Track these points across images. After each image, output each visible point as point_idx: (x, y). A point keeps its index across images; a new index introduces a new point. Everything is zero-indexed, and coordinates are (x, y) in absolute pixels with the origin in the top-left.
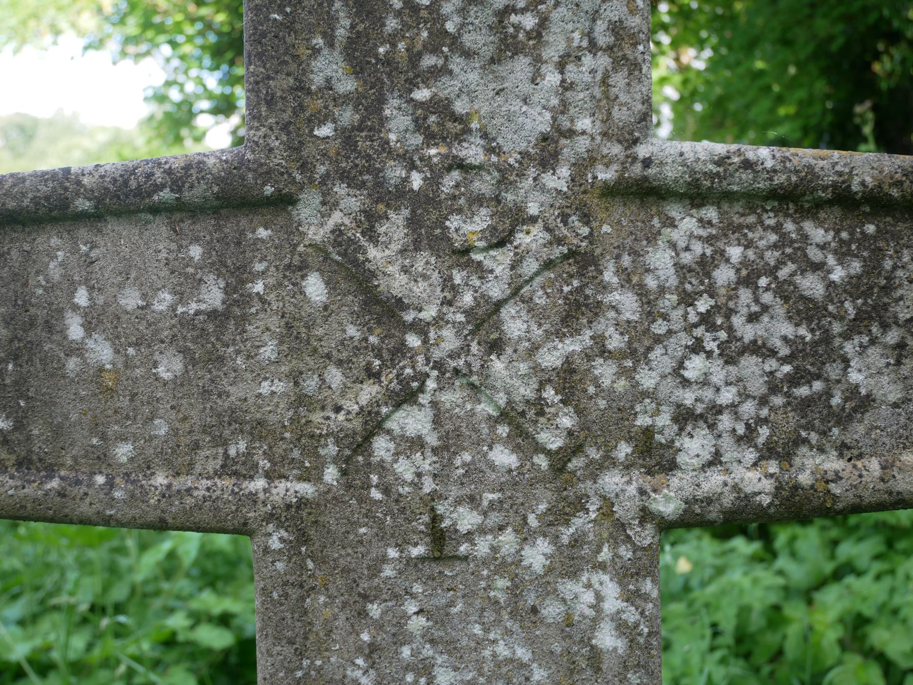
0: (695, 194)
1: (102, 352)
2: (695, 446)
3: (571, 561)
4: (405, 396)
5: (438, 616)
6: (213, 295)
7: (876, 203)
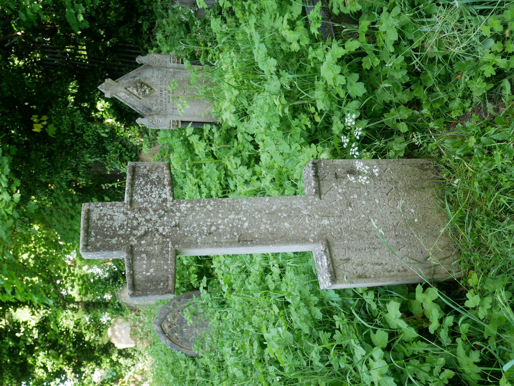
0: (131, 196)
1: (152, 270)
2: (164, 196)
3: (179, 210)
4: (157, 230)
6: (144, 255)
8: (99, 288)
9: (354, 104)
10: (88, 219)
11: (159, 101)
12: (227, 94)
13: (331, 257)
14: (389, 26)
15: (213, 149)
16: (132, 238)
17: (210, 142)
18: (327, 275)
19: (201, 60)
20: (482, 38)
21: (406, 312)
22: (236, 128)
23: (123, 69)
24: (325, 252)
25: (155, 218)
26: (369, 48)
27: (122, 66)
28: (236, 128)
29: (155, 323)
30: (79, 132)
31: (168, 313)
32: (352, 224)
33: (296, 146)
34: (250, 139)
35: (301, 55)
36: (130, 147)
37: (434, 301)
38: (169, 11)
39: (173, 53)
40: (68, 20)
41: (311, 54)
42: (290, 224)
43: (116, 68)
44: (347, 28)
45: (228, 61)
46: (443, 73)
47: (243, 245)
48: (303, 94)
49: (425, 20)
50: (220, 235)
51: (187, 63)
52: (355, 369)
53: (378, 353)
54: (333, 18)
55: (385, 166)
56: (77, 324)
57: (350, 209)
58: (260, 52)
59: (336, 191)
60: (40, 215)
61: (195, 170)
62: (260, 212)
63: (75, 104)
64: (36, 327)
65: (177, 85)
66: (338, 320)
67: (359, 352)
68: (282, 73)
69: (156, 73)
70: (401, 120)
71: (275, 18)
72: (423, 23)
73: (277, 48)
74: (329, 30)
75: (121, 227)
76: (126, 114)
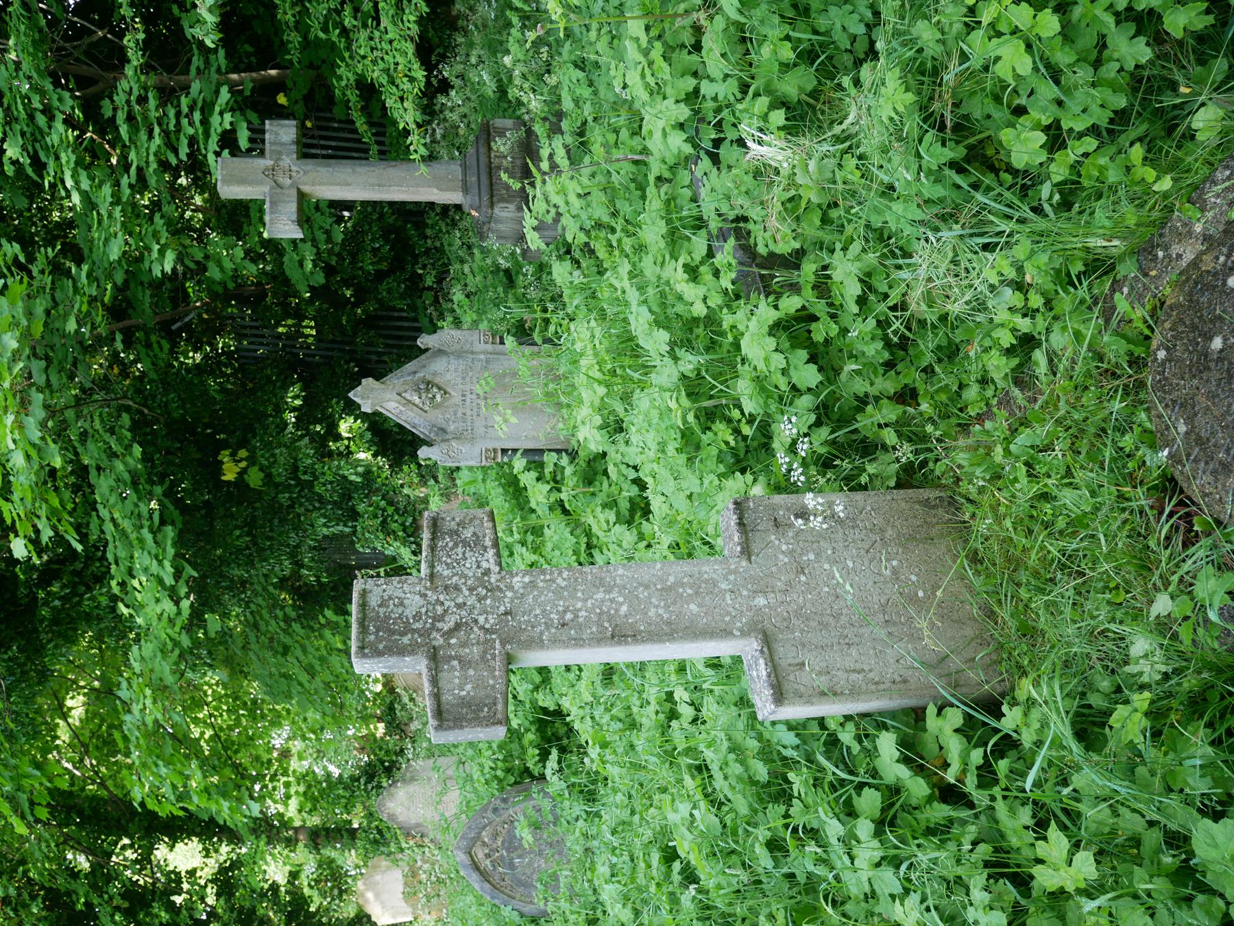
0: (432, 566)
1: (468, 687)
2: (484, 565)
3: (511, 588)
4: (476, 621)
5: (524, 614)
6: (455, 663)
7: (434, 533)
8: (339, 797)
9: (806, 401)
10: (363, 605)
11: (459, 414)
12: (586, 395)
13: (772, 660)
14: (846, 274)
15: (564, 496)
16: (434, 634)
17: (556, 483)
18: (768, 692)
19: (537, 337)
20: (992, 288)
21: (911, 754)
22: (604, 454)
23: (386, 358)
24: (762, 651)
25: (471, 601)
26: (820, 308)
27: (384, 354)
28: (604, 454)
29: (458, 848)
30: (306, 477)
31: (484, 828)
32: (814, 610)
33: (710, 479)
34: (632, 474)
35: (711, 320)
36: (401, 506)
37: (956, 731)
38: (476, 251)
39: (484, 326)
40: (288, 273)
41: (727, 320)
42: (700, 606)
43: (374, 357)
44: (780, 276)
45: (584, 336)
46: (944, 343)
47: (619, 643)
48: (714, 387)
49: (901, 261)
50: (580, 627)
51: (510, 341)
52: (837, 878)
53: (864, 828)
54: (758, 260)
55: (861, 503)
56: (294, 875)
57: (803, 578)
58: (640, 320)
59: (777, 548)
60: (219, 651)
61: (530, 538)
62: (647, 587)
63: (297, 425)
64: (211, 881)
65: (492, 383)
66: (798, 781)
67: (834, 829)
68: (681, 353)
69: (454, 363)
70: (886, 425)
71: (663, 263)
72: (899, 267)
73: (670, 311)
74: (754, 281)
75: (418, 616)
76: (396, 442)
